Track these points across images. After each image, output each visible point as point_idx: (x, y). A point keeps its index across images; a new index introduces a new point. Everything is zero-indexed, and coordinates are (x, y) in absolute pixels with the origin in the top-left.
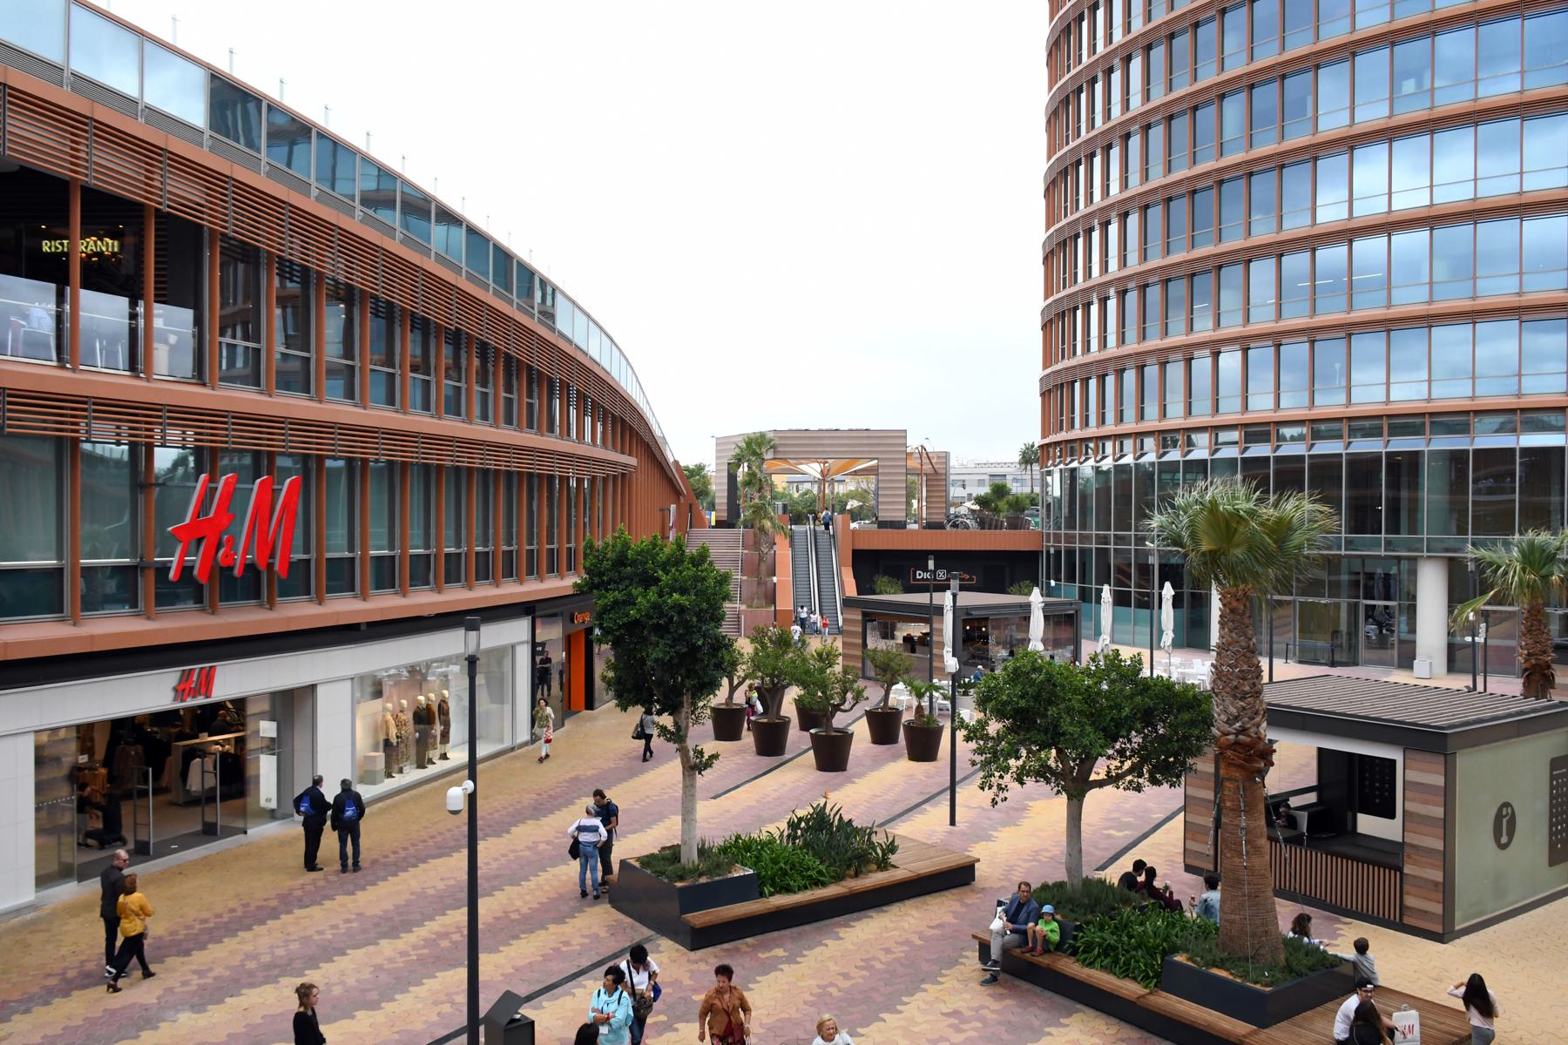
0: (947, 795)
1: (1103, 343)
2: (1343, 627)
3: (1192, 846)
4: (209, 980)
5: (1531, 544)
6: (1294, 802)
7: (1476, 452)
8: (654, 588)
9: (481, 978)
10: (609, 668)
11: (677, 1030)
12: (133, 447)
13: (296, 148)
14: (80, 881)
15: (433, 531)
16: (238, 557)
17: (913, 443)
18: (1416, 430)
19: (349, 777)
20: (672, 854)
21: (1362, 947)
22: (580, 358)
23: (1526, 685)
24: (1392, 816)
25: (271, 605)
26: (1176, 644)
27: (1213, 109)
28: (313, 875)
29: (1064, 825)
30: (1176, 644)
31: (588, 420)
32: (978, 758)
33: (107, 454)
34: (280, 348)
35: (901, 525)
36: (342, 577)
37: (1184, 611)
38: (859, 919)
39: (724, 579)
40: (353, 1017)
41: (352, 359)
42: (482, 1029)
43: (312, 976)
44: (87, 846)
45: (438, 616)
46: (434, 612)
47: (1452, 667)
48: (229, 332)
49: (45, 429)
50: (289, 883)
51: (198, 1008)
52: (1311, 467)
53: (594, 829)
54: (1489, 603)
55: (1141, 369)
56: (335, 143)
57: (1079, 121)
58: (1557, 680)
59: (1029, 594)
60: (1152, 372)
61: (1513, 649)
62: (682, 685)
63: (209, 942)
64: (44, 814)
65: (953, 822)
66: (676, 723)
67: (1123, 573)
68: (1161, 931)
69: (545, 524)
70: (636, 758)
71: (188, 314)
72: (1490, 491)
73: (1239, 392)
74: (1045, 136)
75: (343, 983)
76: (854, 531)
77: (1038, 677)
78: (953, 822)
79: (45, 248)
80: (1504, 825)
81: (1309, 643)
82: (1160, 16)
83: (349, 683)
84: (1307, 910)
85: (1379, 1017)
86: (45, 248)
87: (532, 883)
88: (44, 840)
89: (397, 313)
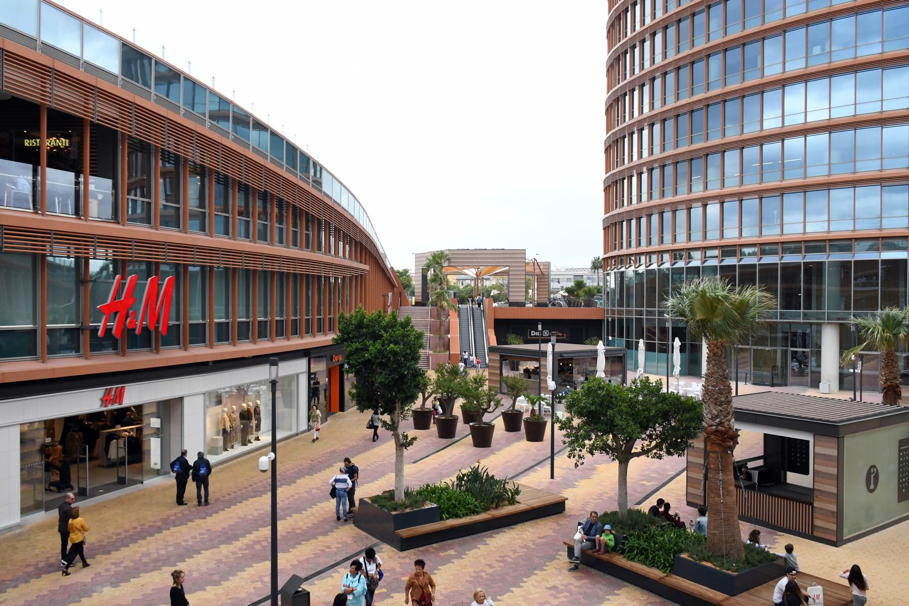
0: (549, 461)
1: (640, 199)
2: (779, 364)
3: (691, 490)
4: (121, 569)
5: (888, 316)
6: (750, 465)
7: (856, 262)
8: (379, 341)
9: (279, 567)
10: (353, 387)
11: (392, 597)
12: (77, 259)
13: (171, 86)
14: (46, 511)
15: (251, 308)
16: (138, 323)
17: (529, 257)
18: (821, 249)
19: (202, 451)
20: (390, 496)
21: (789, 549)
22: (336, 207)
23: (885, 397)
24: (807, 473)
25: (157, 351)
26: (682, 374)
27: (703, 63)
28: (182, 507)
29: (617, 478)
30: (682, 374)
31: (341, 244)
32: (567, 440)
33: (62, 263)
34: (162, 202)
35: (522, 305)
36: (198, 335)
37: (687, 354)
38: (498, 533)
39: (420, 336)
40: (205, 590)
41: (204, 208)
42: (279, 596)
43: (181, 566)
44: (51, 490)
45: (254, 357)
46: (252, 355)
47: (842, 387)
48: (133, 192)
49: (26, 249)
50: (168, 512)
51: (115, 584)
52: (760, 271)
53: (345, 481)
54: (863, 350)
55: (661, 214)
56: (194, 83)
57: (626, 70)
58: (903, 394)
59: (597, 344)
60: (668, 216)
61: (877, 377)
62: (396, 397)
63: (121, 546)
64: (25, 472)
65: (552, 477)
66: (392, 419)
67: (651, 332)
68: (673, 540)
69: (316, 304)
70: (369, 439)
71: (109, 182)
72: (864, 285)
73: (718, 227)
74: (606, 79)
75: (199, 570)
76: (495, 308)
77: (602, 393)
78: (552, 477)
79: (26, 144)
80: (872, 478)
81: (759, 373)
82: (673, 9)
83: (202, 396)
84: (758, 528)
85: (799, 590)
86: (26, 144)
87: (308, 512)
88: (25, 487)
89: (230, 182)
